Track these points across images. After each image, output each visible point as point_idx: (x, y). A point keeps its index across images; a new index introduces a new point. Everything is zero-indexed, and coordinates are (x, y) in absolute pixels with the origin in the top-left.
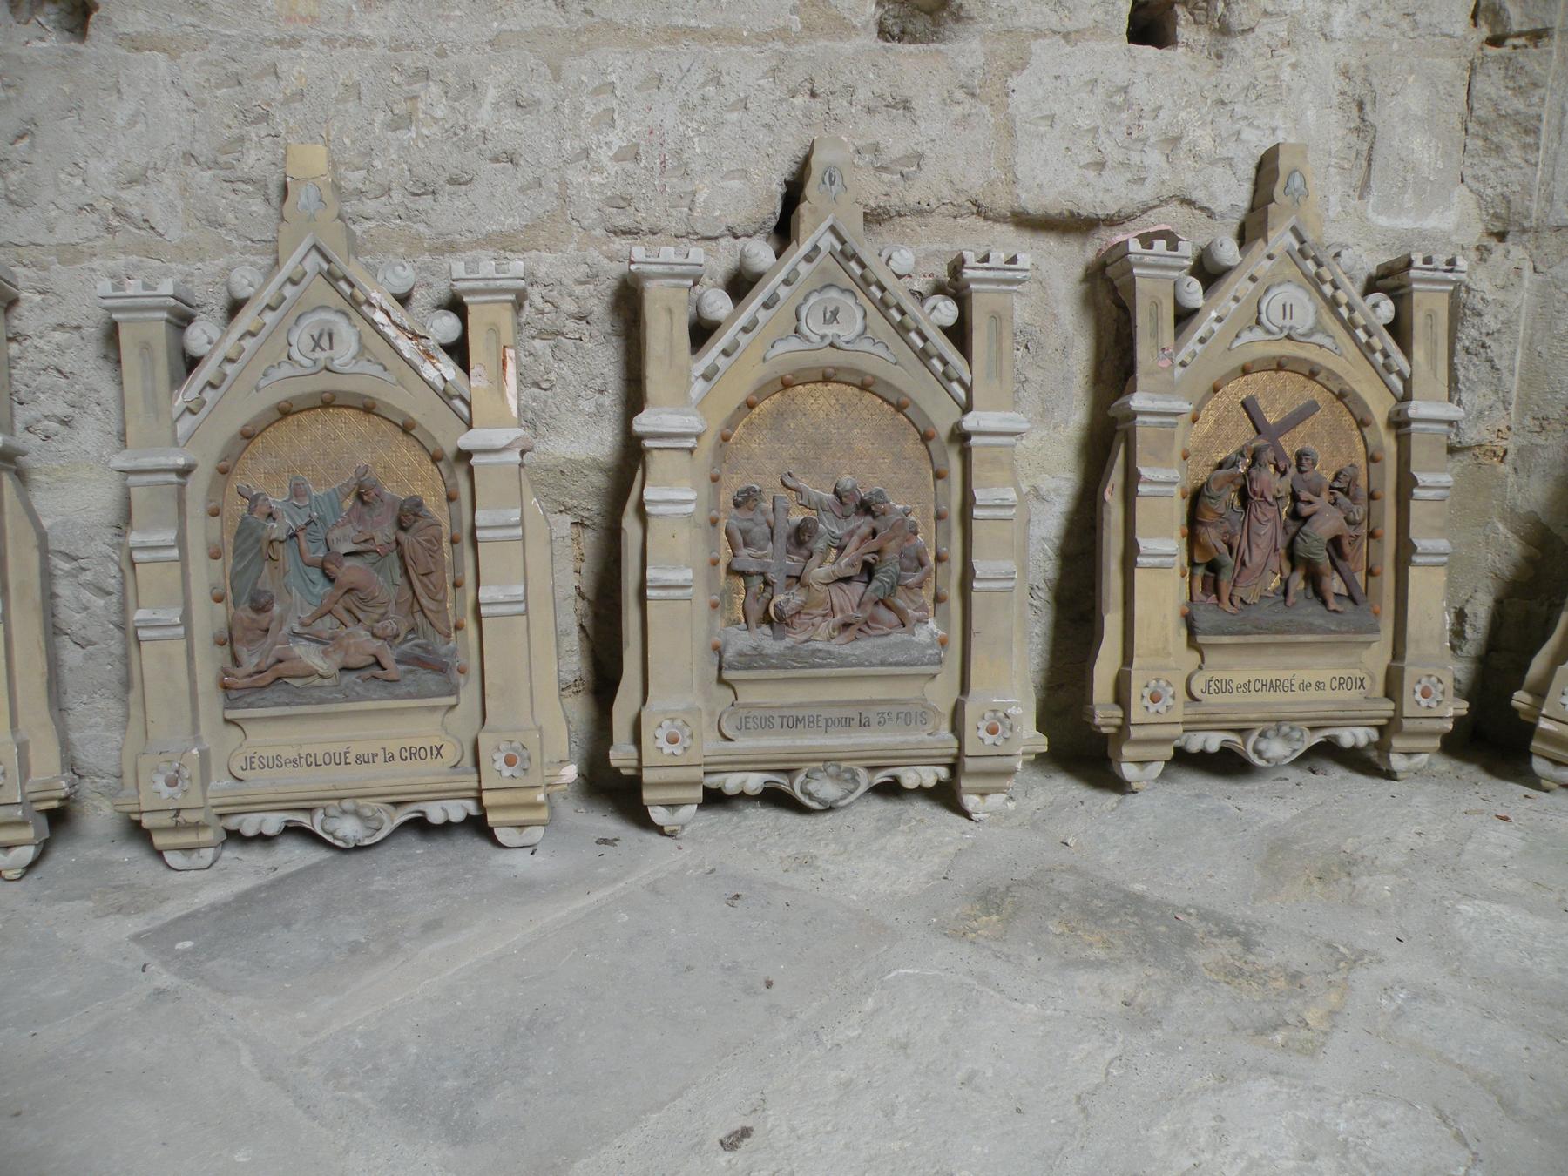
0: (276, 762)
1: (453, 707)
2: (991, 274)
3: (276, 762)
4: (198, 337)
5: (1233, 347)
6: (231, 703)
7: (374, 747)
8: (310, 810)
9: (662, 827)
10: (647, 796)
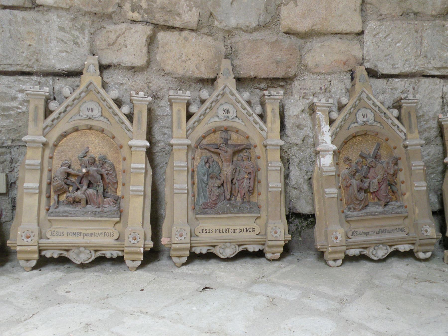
0: (210, 231)
2: (321, 104)
3: (210, 231)
4: (193, 109)
5: (350, 128)
7: (237, 228)
8: (67, 251)
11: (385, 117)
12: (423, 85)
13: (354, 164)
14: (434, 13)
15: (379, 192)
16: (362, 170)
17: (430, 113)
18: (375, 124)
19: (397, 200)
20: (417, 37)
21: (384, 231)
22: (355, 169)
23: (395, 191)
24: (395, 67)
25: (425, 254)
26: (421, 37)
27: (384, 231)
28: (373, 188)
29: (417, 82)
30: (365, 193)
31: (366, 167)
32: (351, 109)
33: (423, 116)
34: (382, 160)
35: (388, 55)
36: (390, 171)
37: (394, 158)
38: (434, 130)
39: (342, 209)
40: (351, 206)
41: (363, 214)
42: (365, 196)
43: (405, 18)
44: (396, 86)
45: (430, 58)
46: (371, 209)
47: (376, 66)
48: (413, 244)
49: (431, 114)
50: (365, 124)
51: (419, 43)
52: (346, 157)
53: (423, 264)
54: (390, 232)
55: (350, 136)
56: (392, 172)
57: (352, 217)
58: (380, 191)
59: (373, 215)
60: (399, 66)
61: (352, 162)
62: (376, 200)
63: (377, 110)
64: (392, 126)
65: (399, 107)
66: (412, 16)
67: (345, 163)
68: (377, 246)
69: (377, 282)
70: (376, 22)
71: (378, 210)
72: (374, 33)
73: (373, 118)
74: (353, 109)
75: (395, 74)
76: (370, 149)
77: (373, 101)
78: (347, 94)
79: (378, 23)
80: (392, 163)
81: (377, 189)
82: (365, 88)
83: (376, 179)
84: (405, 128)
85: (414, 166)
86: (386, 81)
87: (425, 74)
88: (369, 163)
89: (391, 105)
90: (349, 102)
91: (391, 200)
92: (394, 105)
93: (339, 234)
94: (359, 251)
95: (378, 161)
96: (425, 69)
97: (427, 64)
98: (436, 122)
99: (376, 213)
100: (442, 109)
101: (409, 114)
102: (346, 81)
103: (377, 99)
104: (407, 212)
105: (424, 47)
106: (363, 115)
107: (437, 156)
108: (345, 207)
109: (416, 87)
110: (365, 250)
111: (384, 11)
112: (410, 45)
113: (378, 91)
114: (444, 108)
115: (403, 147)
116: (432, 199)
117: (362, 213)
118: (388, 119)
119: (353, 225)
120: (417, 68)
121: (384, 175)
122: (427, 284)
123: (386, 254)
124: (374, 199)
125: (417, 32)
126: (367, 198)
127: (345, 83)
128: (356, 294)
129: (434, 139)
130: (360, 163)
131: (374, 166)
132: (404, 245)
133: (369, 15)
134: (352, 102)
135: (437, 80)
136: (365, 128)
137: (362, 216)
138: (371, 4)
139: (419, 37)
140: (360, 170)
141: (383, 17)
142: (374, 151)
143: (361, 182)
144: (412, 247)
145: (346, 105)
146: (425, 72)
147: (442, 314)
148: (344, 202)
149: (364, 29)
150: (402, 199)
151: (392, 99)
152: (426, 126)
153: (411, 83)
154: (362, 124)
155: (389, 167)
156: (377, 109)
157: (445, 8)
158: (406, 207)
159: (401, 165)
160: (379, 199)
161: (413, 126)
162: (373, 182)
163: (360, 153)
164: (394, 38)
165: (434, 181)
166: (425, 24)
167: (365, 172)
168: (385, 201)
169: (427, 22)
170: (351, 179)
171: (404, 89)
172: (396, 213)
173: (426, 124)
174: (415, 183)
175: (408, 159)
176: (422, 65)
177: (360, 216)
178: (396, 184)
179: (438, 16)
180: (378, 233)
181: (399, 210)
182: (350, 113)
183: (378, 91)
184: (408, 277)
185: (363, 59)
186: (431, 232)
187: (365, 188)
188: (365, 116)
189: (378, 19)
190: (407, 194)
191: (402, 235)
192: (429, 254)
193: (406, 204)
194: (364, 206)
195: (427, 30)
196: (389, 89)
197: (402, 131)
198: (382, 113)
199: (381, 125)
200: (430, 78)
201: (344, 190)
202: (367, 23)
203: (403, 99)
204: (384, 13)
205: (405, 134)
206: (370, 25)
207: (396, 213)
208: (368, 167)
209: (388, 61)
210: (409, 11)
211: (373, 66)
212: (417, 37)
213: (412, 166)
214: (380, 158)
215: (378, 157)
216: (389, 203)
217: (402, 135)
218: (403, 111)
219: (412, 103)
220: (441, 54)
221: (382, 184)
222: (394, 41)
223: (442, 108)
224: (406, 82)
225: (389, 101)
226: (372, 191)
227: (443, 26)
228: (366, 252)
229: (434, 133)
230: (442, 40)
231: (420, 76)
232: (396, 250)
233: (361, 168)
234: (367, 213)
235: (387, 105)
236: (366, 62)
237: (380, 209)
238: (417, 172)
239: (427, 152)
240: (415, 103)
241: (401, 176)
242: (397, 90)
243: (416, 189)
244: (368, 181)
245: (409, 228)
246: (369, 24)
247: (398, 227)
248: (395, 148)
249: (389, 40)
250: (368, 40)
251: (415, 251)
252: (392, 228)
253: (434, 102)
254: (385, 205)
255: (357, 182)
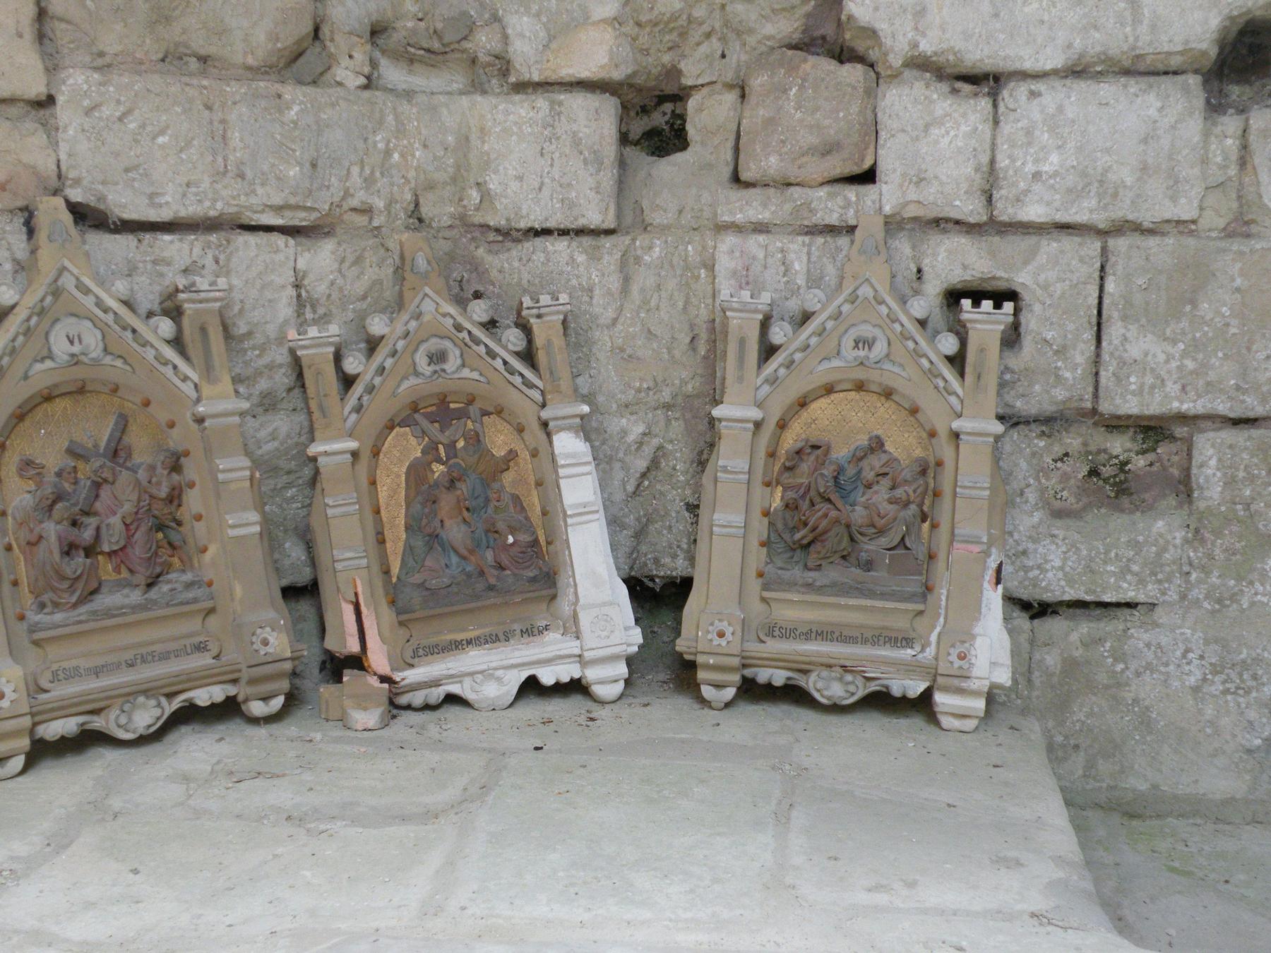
1: (921, 613)
5: (30, 373)
6: (766, 587)
9: (709, 702)
10: (701, 675)
11: (135, 340)
12: (241, 253)
13: (50, 478)
14: (250, 61)
15: (129, 550)
16: (75, 491)
17: (268, 326)
18: (108, 360)
19: (186, 565)
20: (211, 122)
21: (150, 658)
22: (50, 490)
23: (177, 543)
24: (157, 200)
25: (267, 704)
26: (223, 121)
27: (150, 658)
28: (110, 542)
29: (224, 242)
30: (87, 556)
31: (89, 483)
32: (28, 319)
33: (250, 334)
34: (137, 459)
35: (136, 167)
36: (159, 490)
37: (167, 454)
38: (283, 370)
39: (18, 610)
40: (46, 598)
41: (82, 618)
42: (85, 565)
43: (172, 68)
44: (166, 254)
45: (254, 179)
46: (105, 600)
47: (101, 198)
48: (235, 681)
49: (271, 330)
50: (75, 360)
51: (220, 140)
52: (24, 458)
53: (262, 732)
54: (165, 656)
55: (31, 397)
56: (163, 492)
57: (50, 629)
58: (133, 548)
59: (114, 616)
60: (170, 199)
61: (44, 471)
62: (125, 574)
63: (111, 323)
64: (156, 364)
65: (175, 313)
66: (194, 64)
67: (21, 476)
68: (128, 701)
69: (116, 803)
70: (89, 73)
71: (127, 601)
72: (86, 103)
73: (101, 345)
74: (34, 319)
75: (159, 220)
76: (100, 432)
77: (97, 297)
78: (19, 277)
79: (96, 76)
80: (164, 469)
81: (122, 543)
82: (70, 260)
83: (119, 516)
84: (194, 369)
85: (224, 471)
86: (136, 240)
87: (245, 221)
88: (95, 472)
89: (156, 307)
90: (20, 300)
91: (168, 568)
92: (163, 305)
93: (8, 682)
94: (77, 724)
95: (122, 466)
96: (243, 210)
97: (247, 195)
98: (285, 351)
99: (122, 608)
100: (298, 316)
101: (203, 330)
102: (10, 238)
103: (107, 291)
104: (213, 598)
105: (235, 150)
106: (68, 337)
107: (296, 439)
108: (29, 603)
109: (222, 257)
110: (95, 718)
111: (111, 42)
112: (195, 142)
113: (113, 267)
114: (303, 314)
115: (191, 423)
116: (294, 554)
117: (80, 615)
118: (143, 346)
119: (53, 651)
120: (219, 205)
121: (139, 500)
122: (258, 782)
123: (158, 719)
124: (117, 570)
125: (209, 108)
126: (95, 568)
127: (9, 244)
128: (48, 849)
129: (284, 395)
130: (70, 473)
131: (111, 479)
132: (209, 688)
133: (66, 51)
134: (31, 300)
135: (279, 240)
136: (79, 373)
137: (80, 622)
138: (68, 22)
139: (216, 124)
140: (69, 494)
141: (108, 59)
142: (111, 435)
143: (70, 529)
144: (232, 690)
145: (13, 307)
146: (243, 217)
147: (275, 856)
148: (24, 587)
149: (53, 92)
150: (199, 562)
151: (157, 288)
152: (261, 362)
153: (208, 245)
154: (68, 361)
155: (154, 480)
156: (109, 318)
157: (279, 50)
158: (210, 584)
159: (191, 470)
160: (131, 571)
161: (217, 361)
162: (108, 525)
163: (67, 444)
164: (148, 122)
165: (294, 506)
166: (228, 89)
167: (85, 499)
168: (148, 573)
169: (233, 83)
170: (41, 522)
171: (188, 262)
172: (182, 604)
173: (259, 356)
174: (227, 517)
175: (208, 451)
176: (234, 198)
177: (74, 624)
178: (179, 523)
179: (263, 69)
180: (131, 665)
181: (190, 595)
182: (28, 332)
183: (113, 267)
184: (212, 772)
185: (59, 176)
186: (276, 643)
187: (84, 544)
188: (76, 340)
189: (95, 64)
190: (212, 549)
191: (203, 661)
192: (278, 702)
193: (209, 575)
194: (86, 593)
195: (237, 107)
196: (145, 261)
197: (185, 379)
198: (124, 328)
199: (126, 362)
200: (261, 233)
201: (24, 553)
202: (63, 76)
203: (183, 292)
204: (111, 50)
205: (196, 386)
206: (71, 81)
207: (182, 604)
208: (93, 482)
209: (136, 184)
210: (182, 49)
211: (92, 198)
212: (211, 122)
213: (219, 471)
214: (129, 456)
215: (122, 454)
216: (161, 579)
217: (188, 388)
218: (186, 322)
219: (207, 301)
220: (281, 171)
221: (137, 529)
222: (149, 128)
223: (299, 314)
224: (192, 244)
225: (151, 297)
226: (106, 548)
227: (279, 96)
228: (98, 723)
229: (283, 378)
230: (280, 134)
231: (232, 229)
232: (187, 704)
233: (73, 487)
234: (94, 613)
235: (143, 308)
236: (71, 186)
237: (136, 597)
238: (233, 486)
239: (270, 429)
240: (216, 300)
241: (193, 501)
242: (169, 264)
243: (232, 533)
244: (92, 521)
245: (219, 640)
246: (69, 77)
247: (188, 642)
248: (171, 425)
249: (132, 126)
250: (71, 124)
251: (240, 698)
252: (173, 646)
253: (276, 296)
254: (150, 586)
255: (58, 527)
